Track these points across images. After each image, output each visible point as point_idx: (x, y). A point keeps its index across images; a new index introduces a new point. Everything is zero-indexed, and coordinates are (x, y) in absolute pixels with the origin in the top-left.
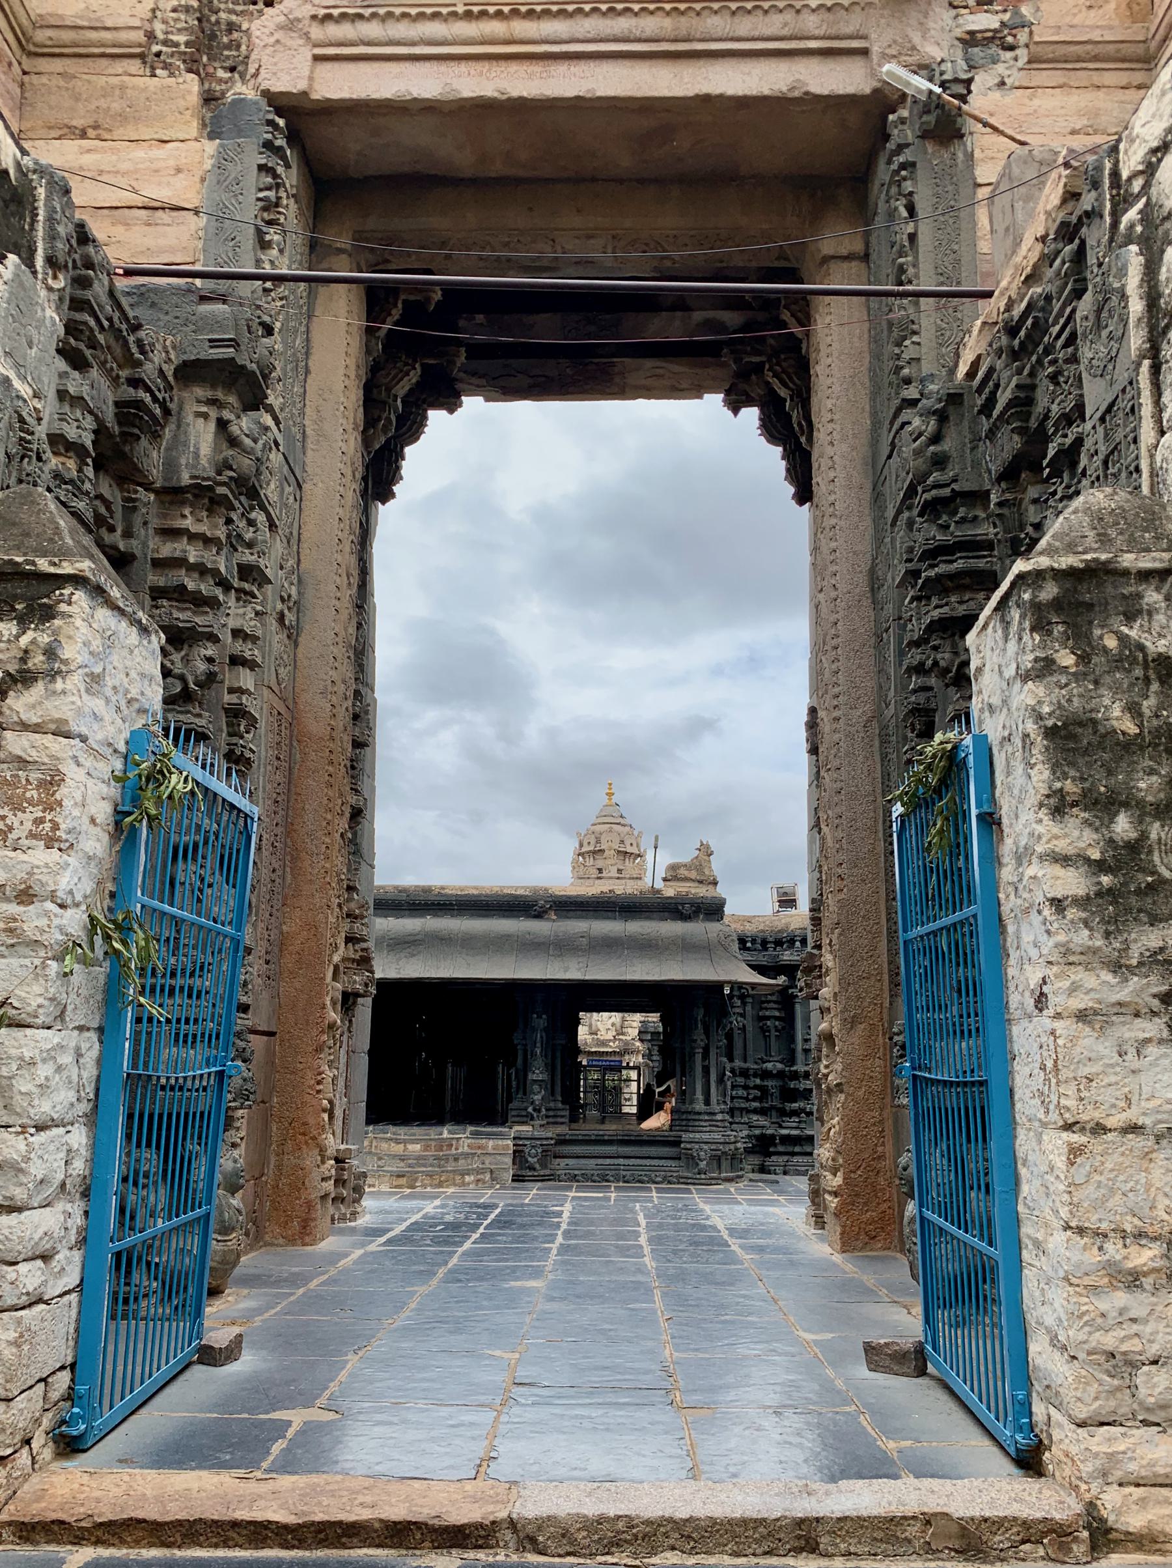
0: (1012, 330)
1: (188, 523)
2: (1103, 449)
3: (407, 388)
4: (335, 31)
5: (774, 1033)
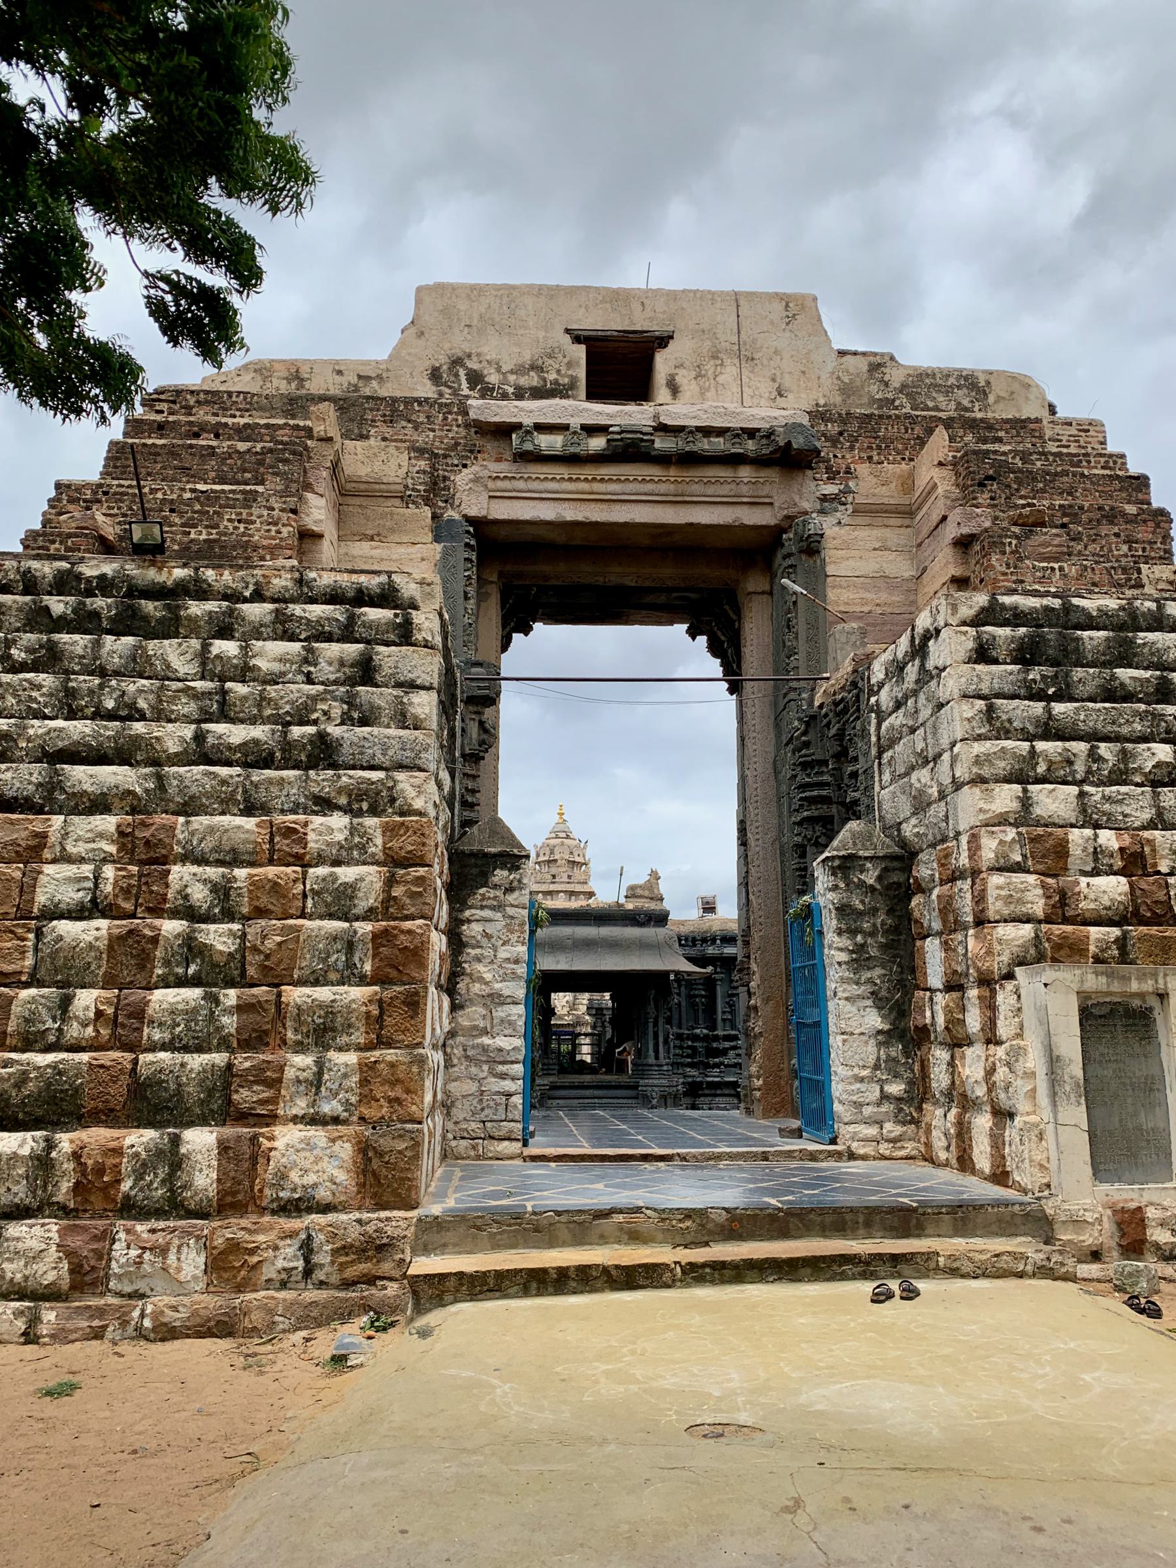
5: (701, 1007)
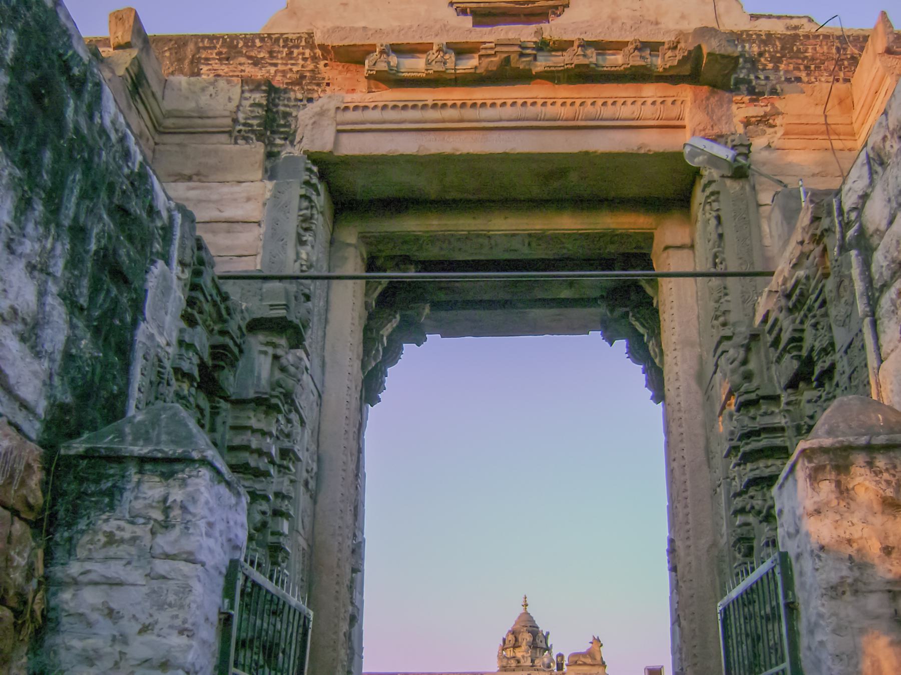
0: (788, 296)
1: (253, 423)
2: (848, 371)
3: (390, 330)
4: (350, 116)
